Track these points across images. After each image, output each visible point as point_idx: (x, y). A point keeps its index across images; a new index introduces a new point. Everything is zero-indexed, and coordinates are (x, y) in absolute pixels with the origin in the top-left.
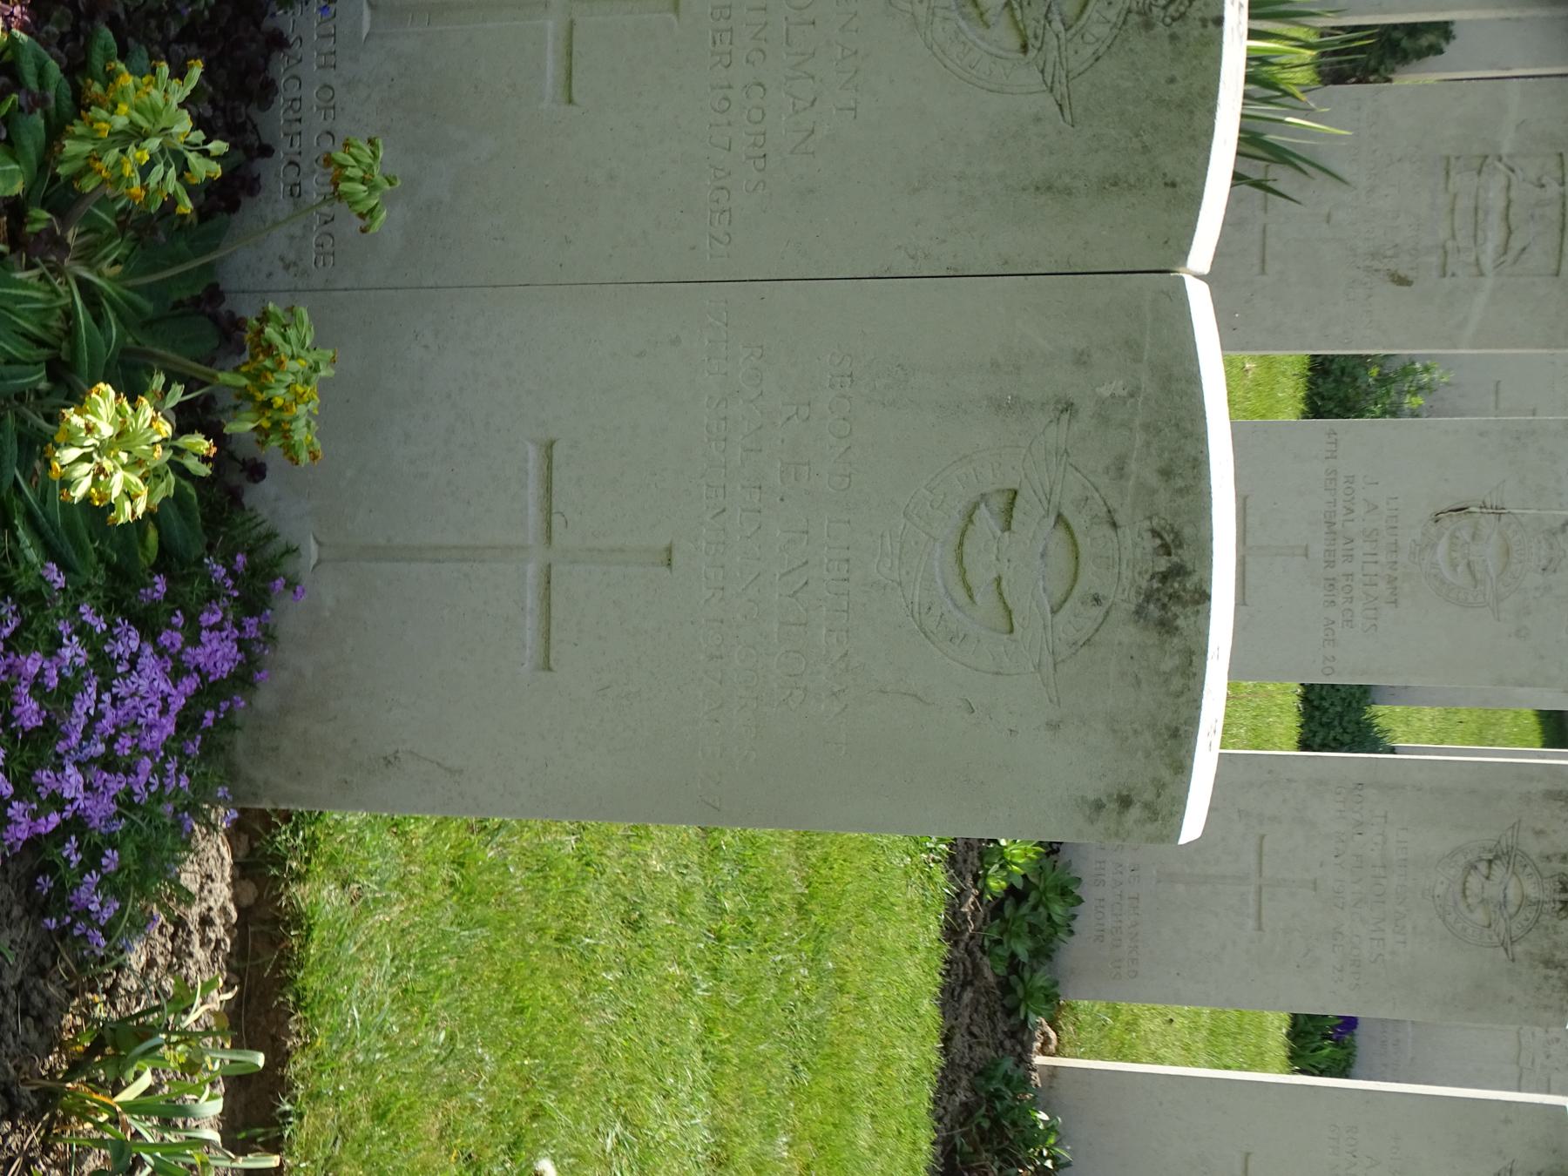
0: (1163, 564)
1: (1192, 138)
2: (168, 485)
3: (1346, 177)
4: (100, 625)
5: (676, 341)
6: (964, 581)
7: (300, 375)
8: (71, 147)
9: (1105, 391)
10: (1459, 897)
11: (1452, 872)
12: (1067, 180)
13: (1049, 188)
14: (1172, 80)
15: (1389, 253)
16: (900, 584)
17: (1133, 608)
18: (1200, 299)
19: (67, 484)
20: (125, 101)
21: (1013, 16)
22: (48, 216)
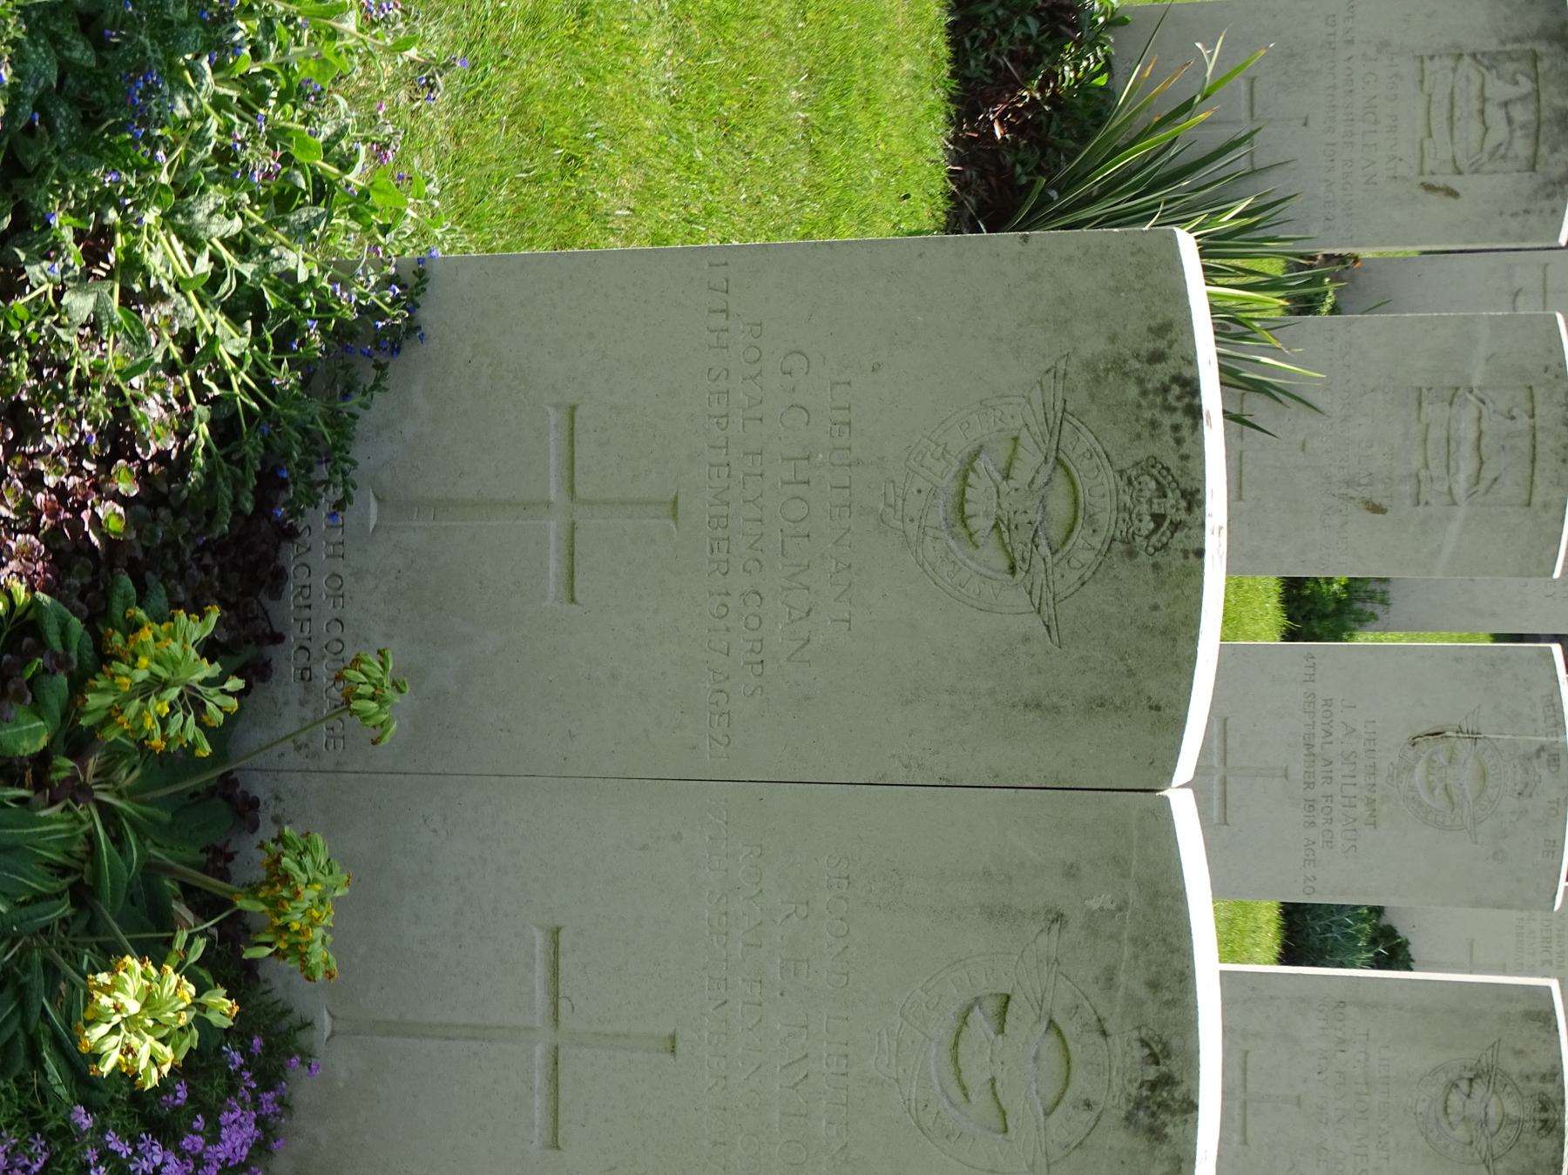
0: (1152, 1073)
1: (1176, 664)
2: (192, 1039)
3: (1320, 406)
4: (125, 1150)
5: (677, 837)
6: (959, 1079)
7: (315, 905)
8: (93, 701)
9: (1094, 904)
10: (1441, 1114)
11: (1434, 1090)
12: (1055, 699)
13: (1038, 706)
14: (1155, 608)
15: (1364, 481)
16: (897, 1081)
17: (1123, 1114)
18: (1183, 805)
19: (97, 1058)
20: (145, 654)
21: (1001, 538)
22: (71, 764)
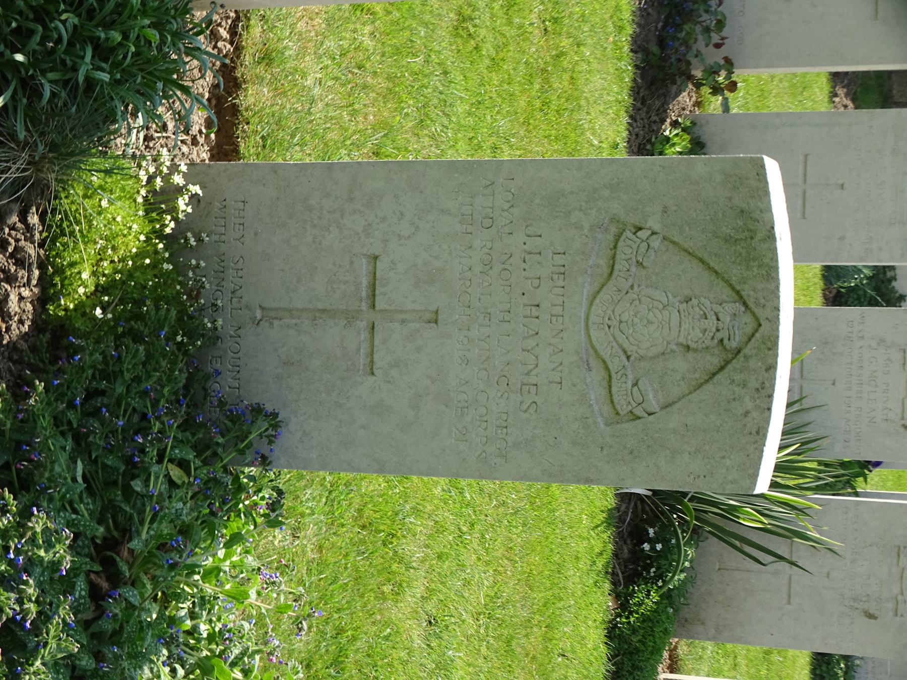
15: (864, 599)
